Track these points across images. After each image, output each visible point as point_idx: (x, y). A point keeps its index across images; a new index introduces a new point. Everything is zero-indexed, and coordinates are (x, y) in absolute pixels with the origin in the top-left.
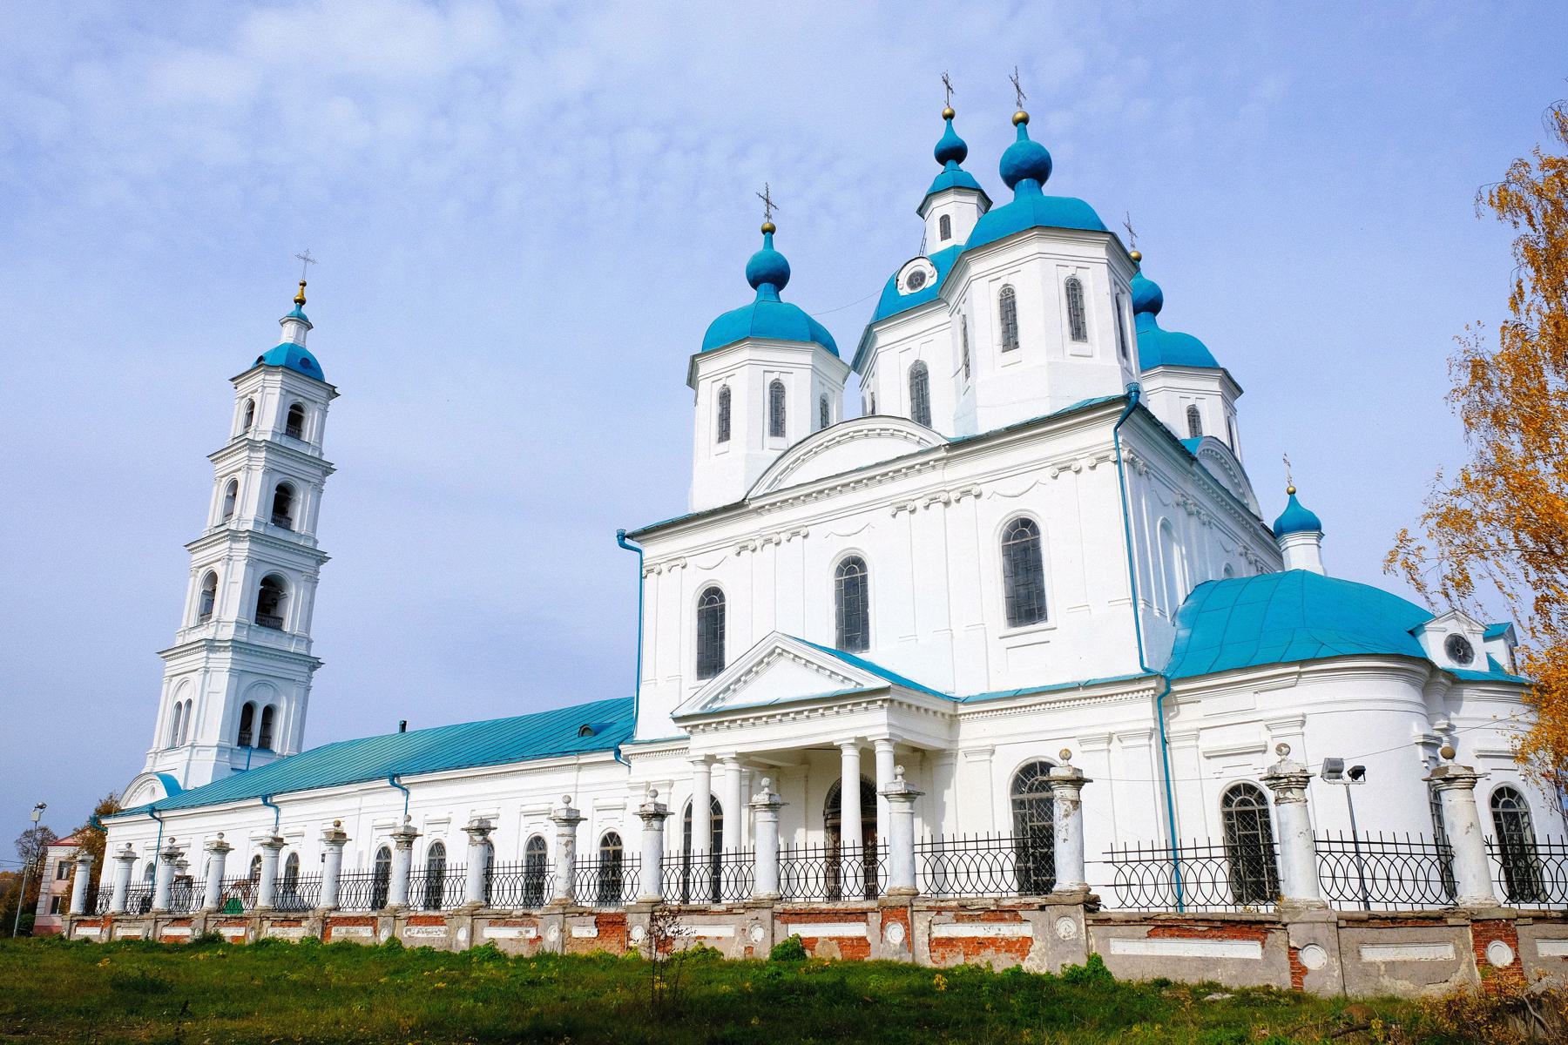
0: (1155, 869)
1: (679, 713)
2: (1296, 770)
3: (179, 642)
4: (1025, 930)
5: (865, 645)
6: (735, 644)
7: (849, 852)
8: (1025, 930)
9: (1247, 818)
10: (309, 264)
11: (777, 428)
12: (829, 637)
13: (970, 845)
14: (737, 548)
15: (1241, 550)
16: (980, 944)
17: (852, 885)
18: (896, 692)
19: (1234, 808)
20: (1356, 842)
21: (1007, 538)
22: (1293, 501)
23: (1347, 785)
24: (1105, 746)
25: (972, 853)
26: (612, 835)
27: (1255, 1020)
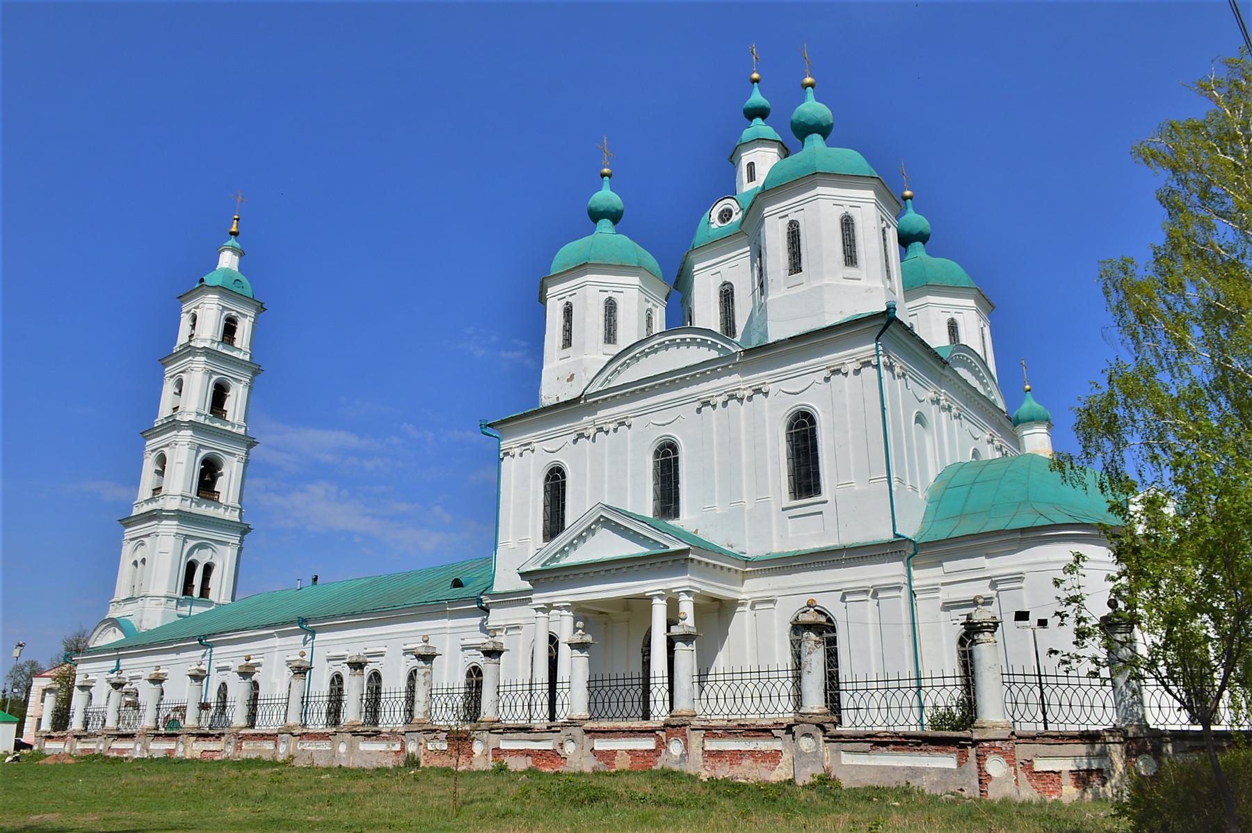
0: (1026, 690)
1: (524, 570)
3: (136, 512)
4: (777, 745)
5: (676, 514)
7: (658, 680)
8: (777, 745)
11: (610, 337)
12: (648, 510)
14: (574, 436)
15: (987, 437)
16: (738, 755)
17: (542, 712)
21: (790, 427)
25: (773, 681)
26: (475, 668)
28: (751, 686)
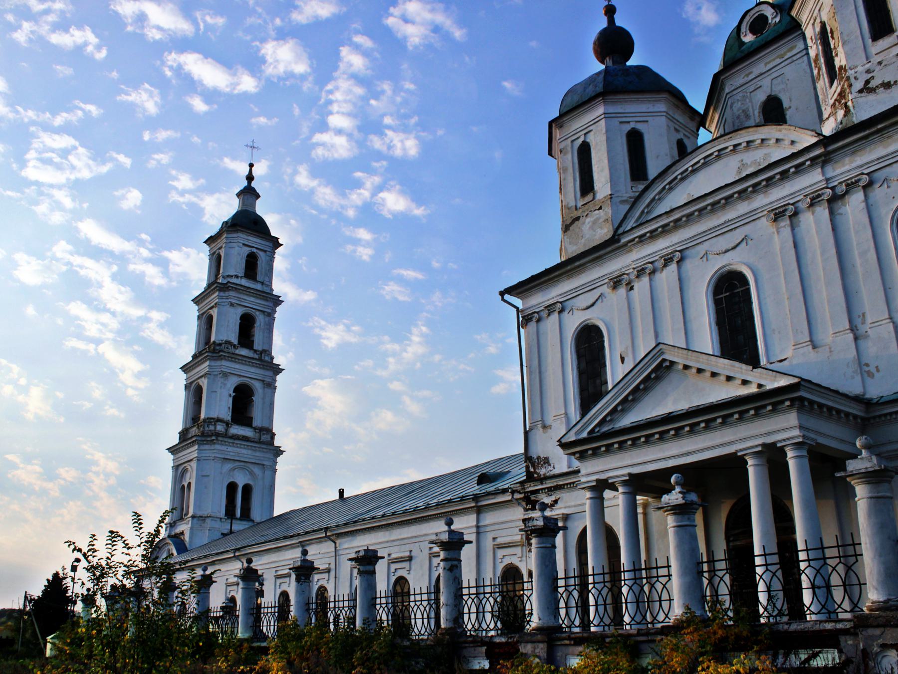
6: (615, 371)
10: (255, 150)
27: (532, 483)
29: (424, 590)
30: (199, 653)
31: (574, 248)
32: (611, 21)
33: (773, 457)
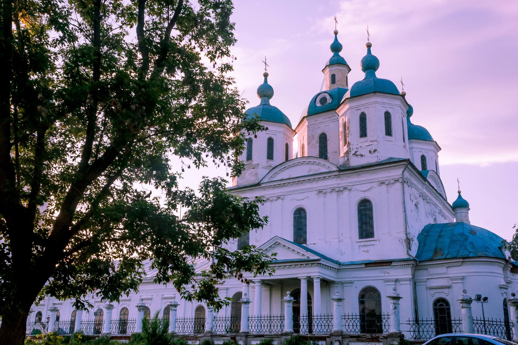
2: (469, 298)
7: (315, 317)
9: (442, 311)
13: (275, 318)
18: (320, 260)
19: (438, 307)
20: (484, 321)
22: (460, 196)
23: (482, 303)
24: (394, 283)
28: (255, 322)
29: (194, 318)
30: (29, 53)
31: (241, 181)
32: (369, 51)
33: (310, 282)
